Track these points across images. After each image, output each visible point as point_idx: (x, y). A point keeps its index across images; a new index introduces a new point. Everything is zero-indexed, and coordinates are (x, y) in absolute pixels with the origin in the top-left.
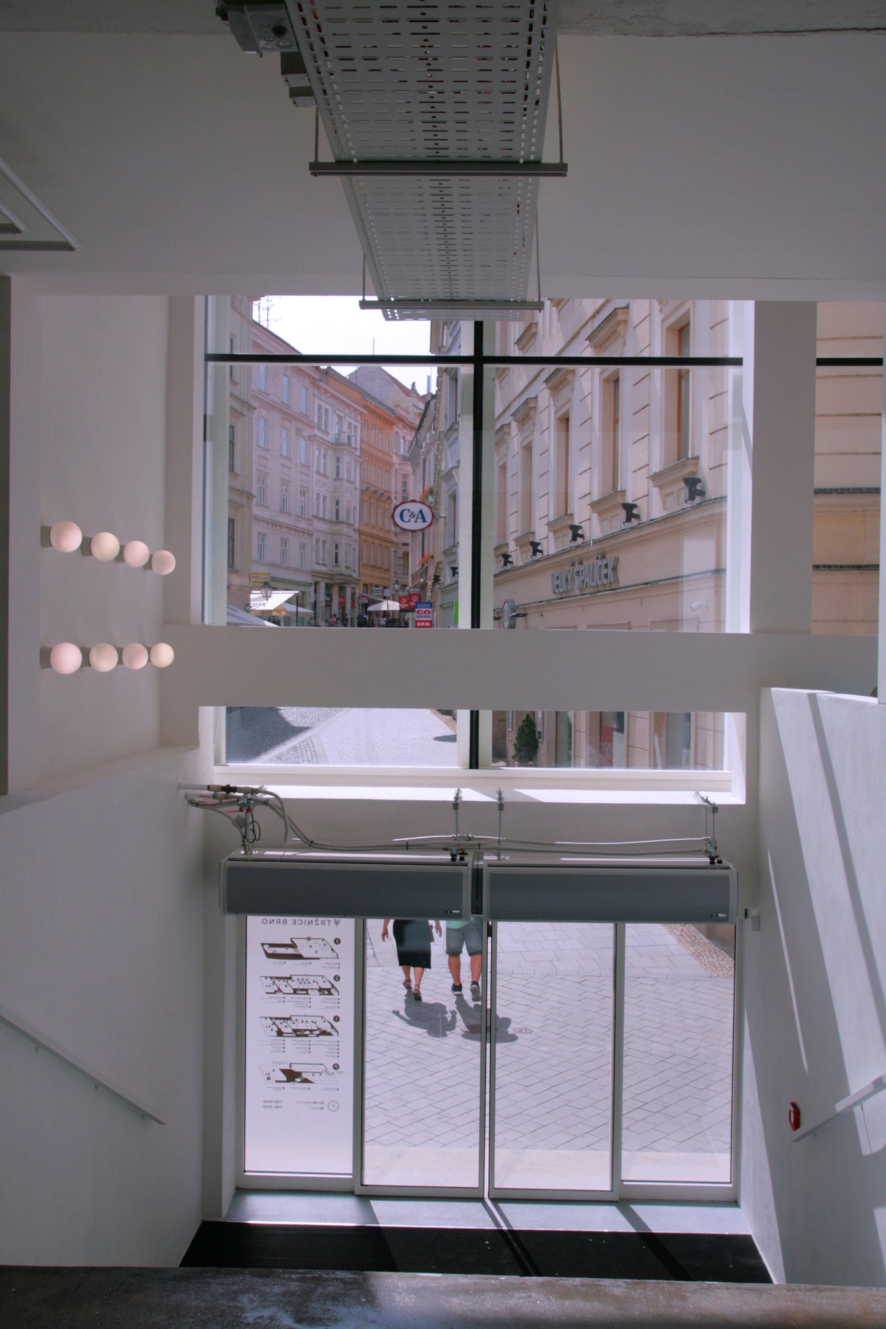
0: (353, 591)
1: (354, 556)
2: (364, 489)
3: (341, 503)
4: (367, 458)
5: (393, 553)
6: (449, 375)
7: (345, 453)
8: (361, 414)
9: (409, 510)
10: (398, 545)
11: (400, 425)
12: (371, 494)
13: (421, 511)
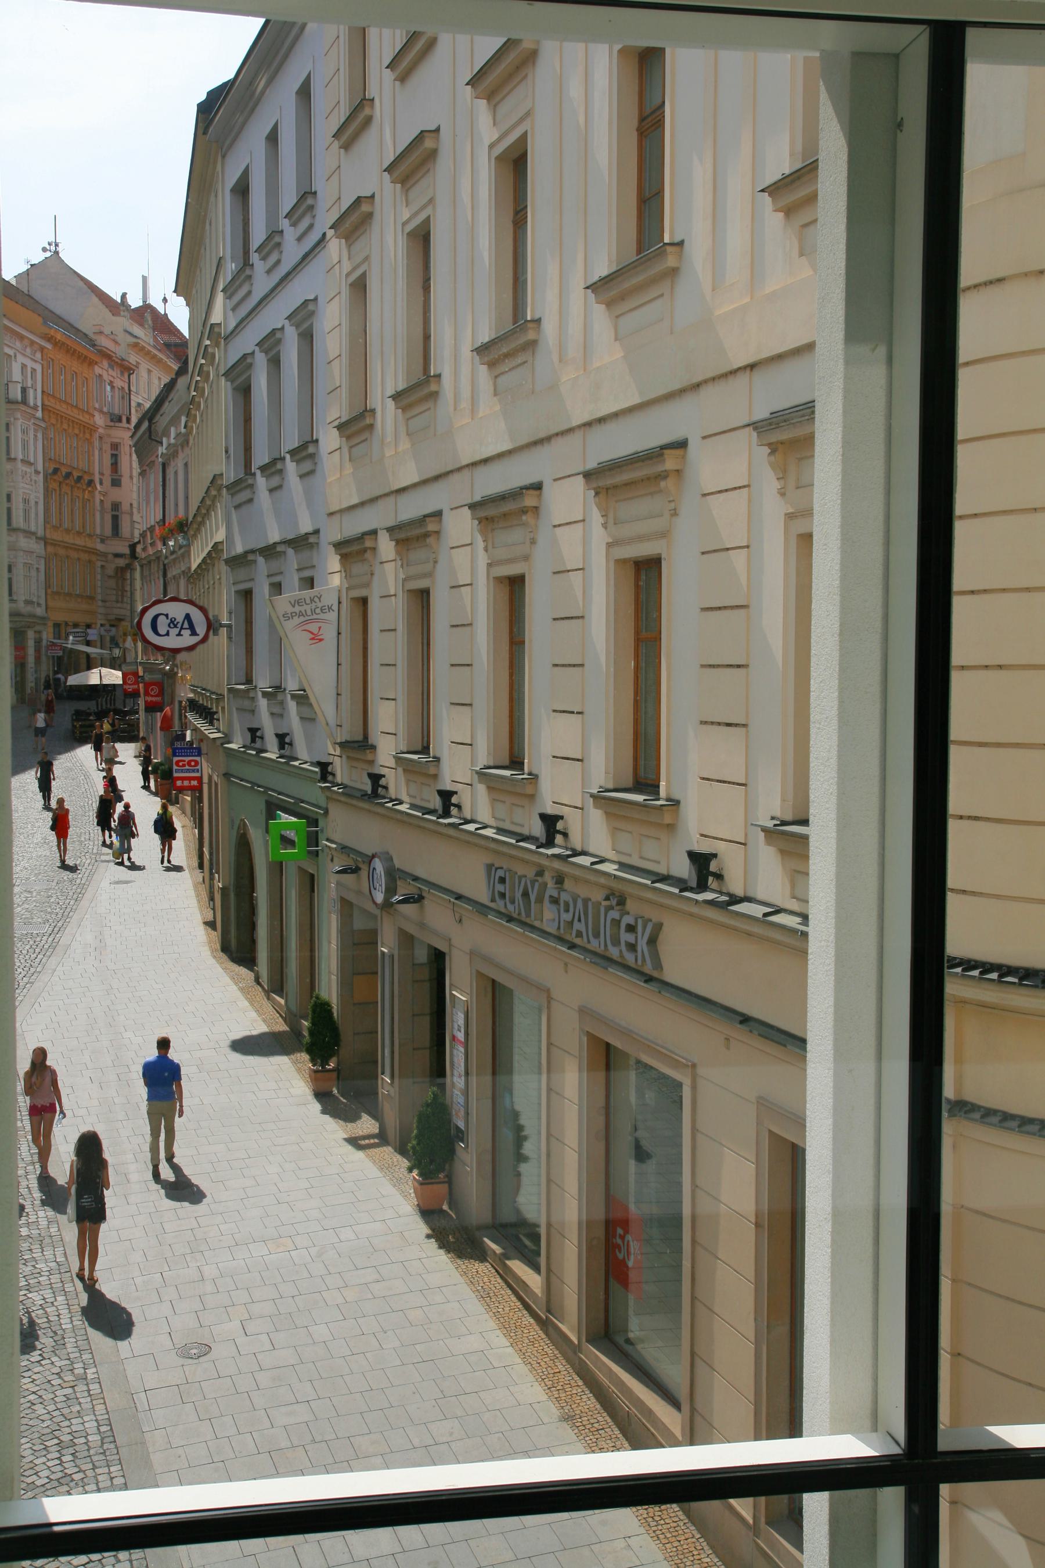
0: (37, 636)
1: (37, 580)
2: (51, 471)
3: (13, 497)
4: (53, 421)
5: (99, 570)
6: (232, 382)
7: (19, 415)
8: (42, 349)
9: (167, 616)
10: (106, 557)
11: (105, 364)
12: (61, 479)
13: (188, 617)
